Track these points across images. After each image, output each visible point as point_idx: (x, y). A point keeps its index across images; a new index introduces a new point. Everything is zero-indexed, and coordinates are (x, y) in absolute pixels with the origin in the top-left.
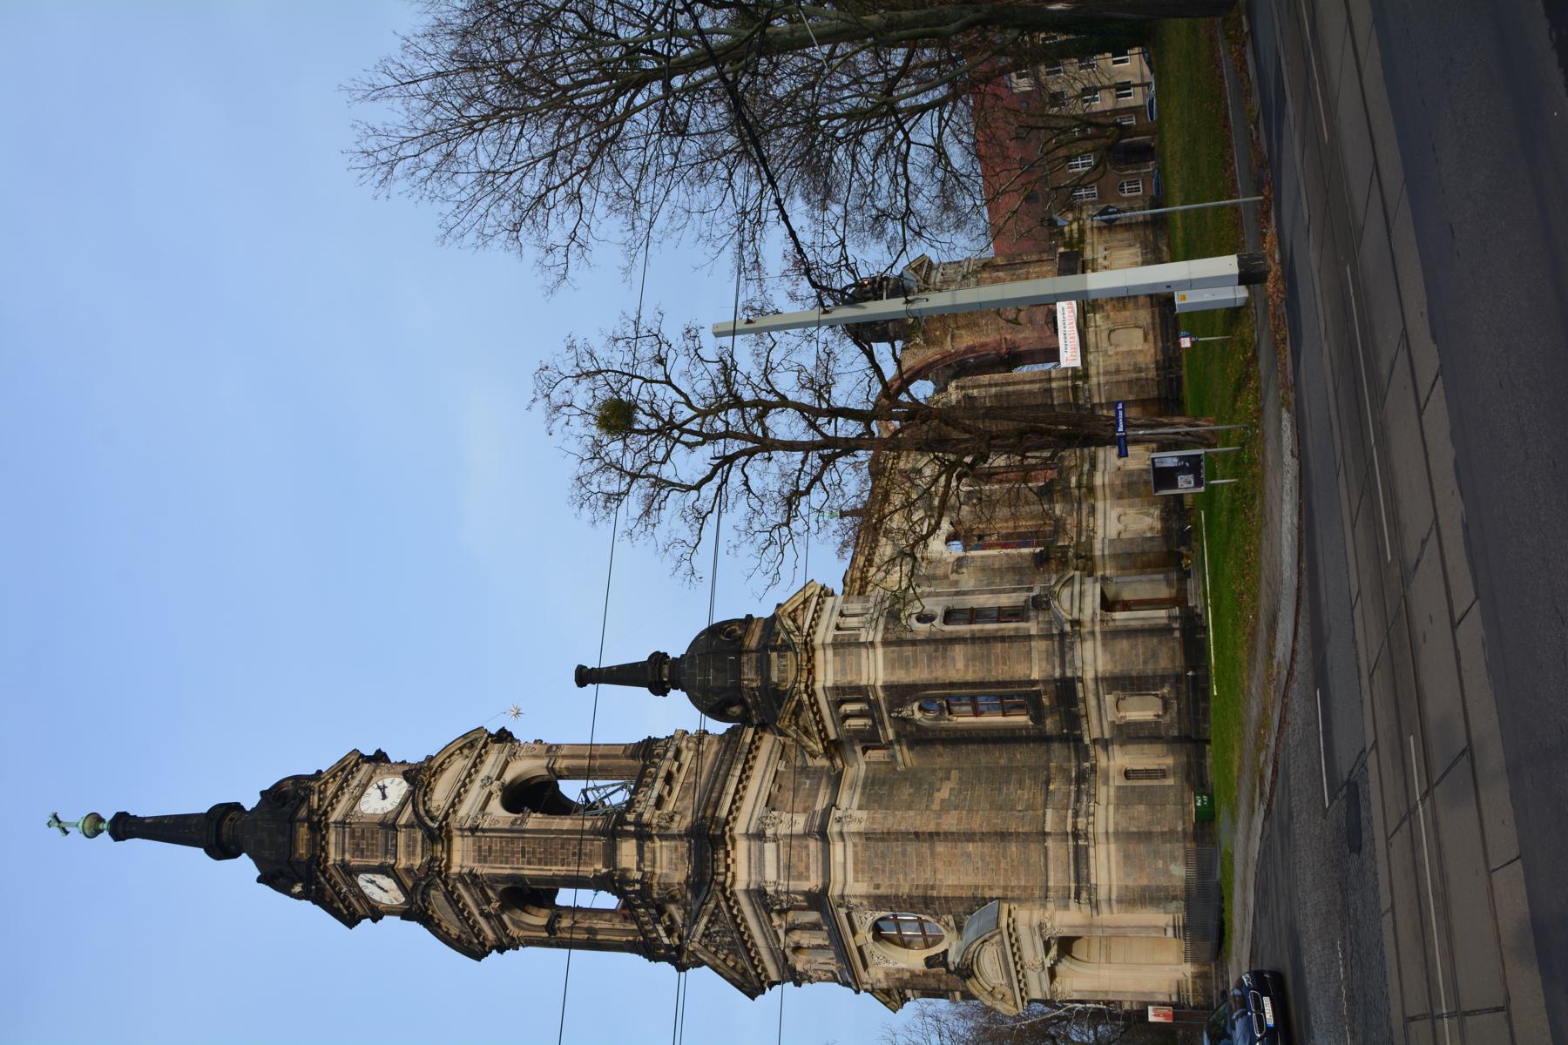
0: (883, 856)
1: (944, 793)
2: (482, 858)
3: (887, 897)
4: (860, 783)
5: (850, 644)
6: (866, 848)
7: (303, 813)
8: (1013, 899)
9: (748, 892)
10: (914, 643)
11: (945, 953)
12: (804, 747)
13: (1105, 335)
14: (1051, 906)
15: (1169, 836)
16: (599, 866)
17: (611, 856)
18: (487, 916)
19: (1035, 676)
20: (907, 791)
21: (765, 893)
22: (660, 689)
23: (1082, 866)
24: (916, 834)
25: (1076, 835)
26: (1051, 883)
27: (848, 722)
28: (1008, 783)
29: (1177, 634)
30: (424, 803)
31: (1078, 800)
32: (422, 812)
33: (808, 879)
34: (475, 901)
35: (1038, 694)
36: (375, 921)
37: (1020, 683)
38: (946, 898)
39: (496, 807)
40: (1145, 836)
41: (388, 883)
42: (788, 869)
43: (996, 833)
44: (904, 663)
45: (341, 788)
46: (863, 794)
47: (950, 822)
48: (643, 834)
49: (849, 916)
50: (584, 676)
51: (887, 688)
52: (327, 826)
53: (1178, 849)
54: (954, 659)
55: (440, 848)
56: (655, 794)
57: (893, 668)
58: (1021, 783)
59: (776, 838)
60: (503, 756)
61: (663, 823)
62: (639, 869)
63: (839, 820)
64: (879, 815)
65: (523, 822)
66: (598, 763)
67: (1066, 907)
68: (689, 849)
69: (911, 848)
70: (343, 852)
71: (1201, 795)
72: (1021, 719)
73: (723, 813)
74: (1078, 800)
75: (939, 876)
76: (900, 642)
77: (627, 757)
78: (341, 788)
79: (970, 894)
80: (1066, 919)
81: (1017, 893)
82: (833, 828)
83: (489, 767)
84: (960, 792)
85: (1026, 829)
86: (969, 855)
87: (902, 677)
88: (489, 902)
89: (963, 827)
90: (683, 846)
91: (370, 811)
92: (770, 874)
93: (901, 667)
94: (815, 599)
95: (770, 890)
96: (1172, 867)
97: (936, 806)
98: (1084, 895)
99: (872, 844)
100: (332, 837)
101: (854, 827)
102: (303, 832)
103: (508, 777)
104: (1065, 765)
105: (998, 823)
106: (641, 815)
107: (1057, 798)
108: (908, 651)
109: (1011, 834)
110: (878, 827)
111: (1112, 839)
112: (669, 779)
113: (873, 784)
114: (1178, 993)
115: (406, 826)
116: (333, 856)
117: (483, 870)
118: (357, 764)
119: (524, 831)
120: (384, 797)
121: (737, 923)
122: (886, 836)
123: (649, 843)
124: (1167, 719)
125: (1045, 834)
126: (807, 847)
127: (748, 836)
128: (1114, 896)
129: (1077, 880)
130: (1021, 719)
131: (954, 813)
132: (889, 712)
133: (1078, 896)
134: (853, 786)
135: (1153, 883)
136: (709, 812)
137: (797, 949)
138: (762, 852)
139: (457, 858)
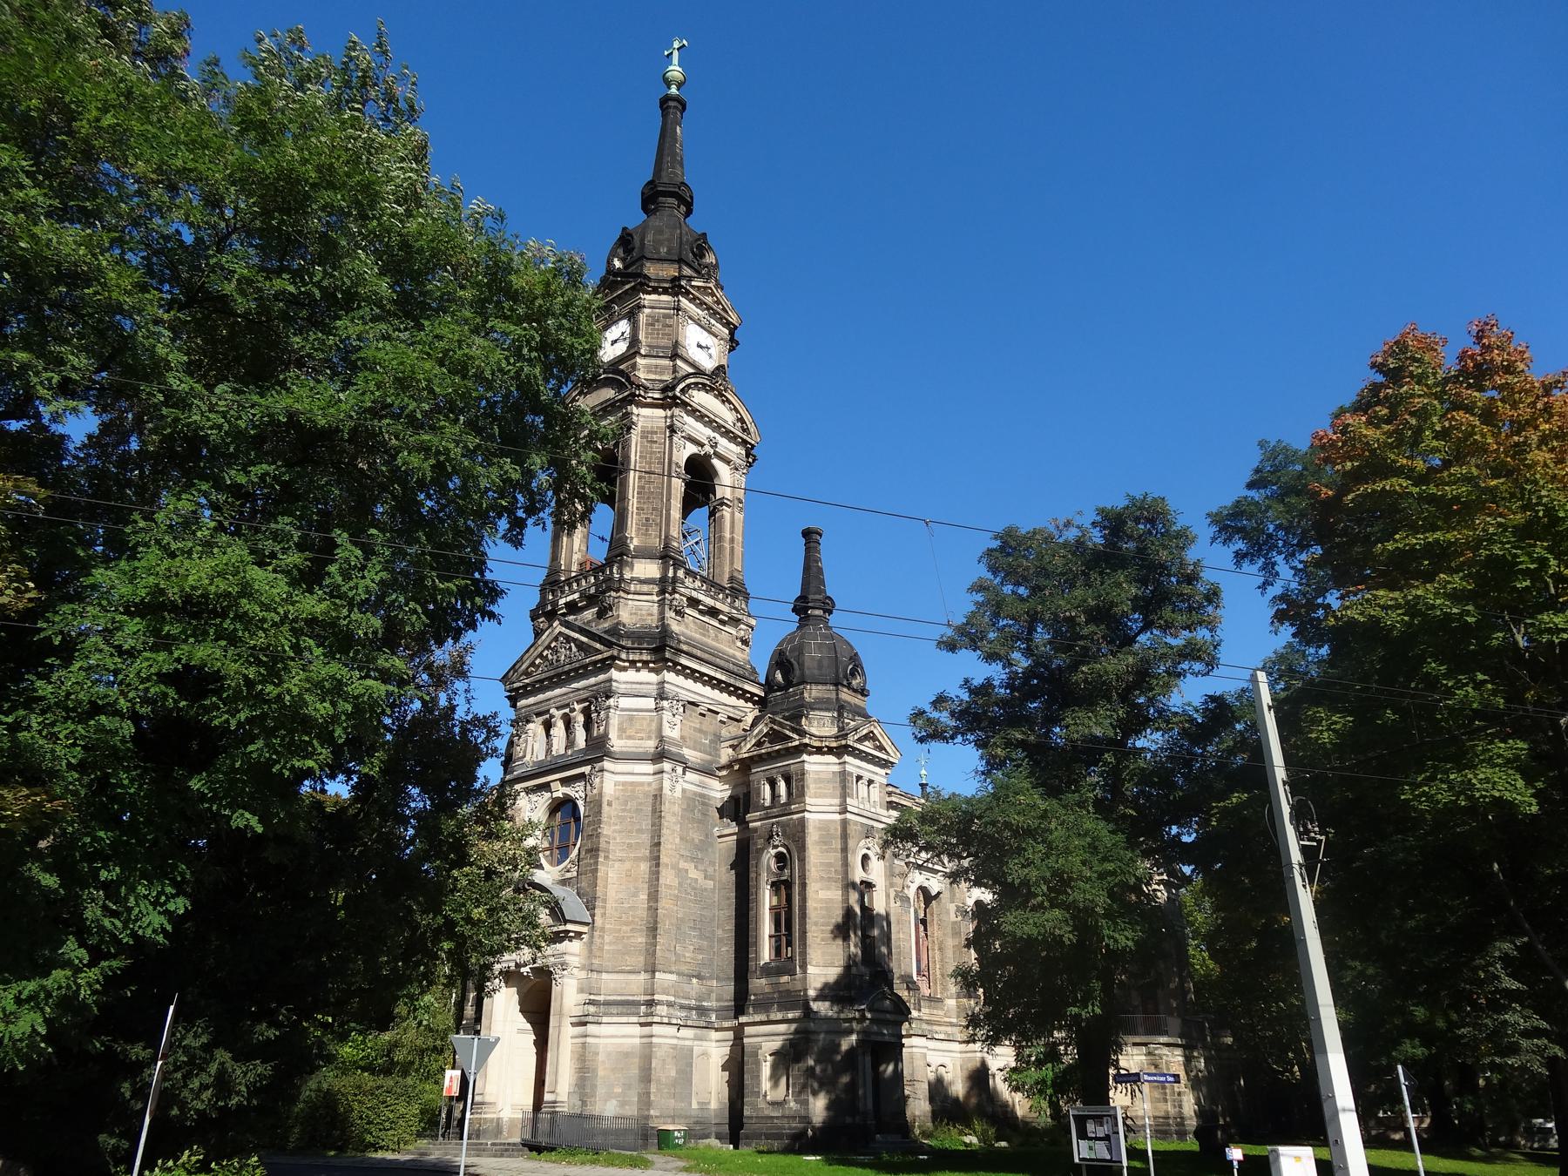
1: (694, 874)
2: (645, 434)
4: (705, 791)
5: (844, 788)
6: (646, 794)
7: (687, 271)
8: (592, 937)
9: (610, 680)
10: (845, 850)
11: (541, 867)
14: (583, 974)
15: (645, 1100)
16: (636, 542)
19: (810, 969)
20: (697, 836)
21: (608, 697)
24: (659, 844)
26: (604, 976)
27: (767, 787)
28: (701, 937)
29: (849, 1120)
30: (696, 384)
31: (682, 1007)
32: (688, 381)
33: (620, 737)
35: (792, 973)
37: (804, 954)
38: (596, 870)
39: (691, 449)
40: (646, 1076)
41: (622, 348)
42: (631, 716)
43: (656, 922)
44: (824, 841)
45: (709, 308)
47: (668, 877)
48: (665, 586)
49: (582, 776)
51: (802, 821)
52: (676, 294)
53: (632, 1110)
56: (701, 597)
57: (820, 829)
58: (699, 950)
60: (734, 458)
62: (632, 579)
64: (676, 808)
66: (727, 545)
67: (581, 991)
69: (645, 838)
72: (766, 954)
74: (682, 1007)
75: (617, 864)
76: (845, 836)
77: (731, 572)
78: (709, 308)
79: (599, 894)
80: (568, 996)
81: (597, 940)
82: (667, 766)
83: (725, 445)
85: (659, 953)
86: (635, 895)
87: (812, 837)
89: (662, 889)
93: (821, 836)
95: (611, 702)
96: (614, 1102)
97: (682, 865)
98: (592, 1009)
99: (650, 800)
100: (665, 298)
101: (667, 784)
102: (671, 271)
103: (716, 462)
104: (714, 996)
107: (686, 987)
108: (837, 844)
109: (655, 937)
110: (666, 807)
112: (713, 612)
113: (704, 804)
116: (648, 299)
117: (635, 437)
119: (670, 476)
120: (699, 346)
121: (582, 672)
122: (657, 814)
123: (656, 589)
124: (762, 1105)
125: (653, 972)
126: (649, 738)
128: (589, 1040)
129: (607, 1003)
130: (766, 954)
131: (676, 883)
133: (591, 1003)
135: (599, 1082)
136: (685, 648)
137: (548, 726)
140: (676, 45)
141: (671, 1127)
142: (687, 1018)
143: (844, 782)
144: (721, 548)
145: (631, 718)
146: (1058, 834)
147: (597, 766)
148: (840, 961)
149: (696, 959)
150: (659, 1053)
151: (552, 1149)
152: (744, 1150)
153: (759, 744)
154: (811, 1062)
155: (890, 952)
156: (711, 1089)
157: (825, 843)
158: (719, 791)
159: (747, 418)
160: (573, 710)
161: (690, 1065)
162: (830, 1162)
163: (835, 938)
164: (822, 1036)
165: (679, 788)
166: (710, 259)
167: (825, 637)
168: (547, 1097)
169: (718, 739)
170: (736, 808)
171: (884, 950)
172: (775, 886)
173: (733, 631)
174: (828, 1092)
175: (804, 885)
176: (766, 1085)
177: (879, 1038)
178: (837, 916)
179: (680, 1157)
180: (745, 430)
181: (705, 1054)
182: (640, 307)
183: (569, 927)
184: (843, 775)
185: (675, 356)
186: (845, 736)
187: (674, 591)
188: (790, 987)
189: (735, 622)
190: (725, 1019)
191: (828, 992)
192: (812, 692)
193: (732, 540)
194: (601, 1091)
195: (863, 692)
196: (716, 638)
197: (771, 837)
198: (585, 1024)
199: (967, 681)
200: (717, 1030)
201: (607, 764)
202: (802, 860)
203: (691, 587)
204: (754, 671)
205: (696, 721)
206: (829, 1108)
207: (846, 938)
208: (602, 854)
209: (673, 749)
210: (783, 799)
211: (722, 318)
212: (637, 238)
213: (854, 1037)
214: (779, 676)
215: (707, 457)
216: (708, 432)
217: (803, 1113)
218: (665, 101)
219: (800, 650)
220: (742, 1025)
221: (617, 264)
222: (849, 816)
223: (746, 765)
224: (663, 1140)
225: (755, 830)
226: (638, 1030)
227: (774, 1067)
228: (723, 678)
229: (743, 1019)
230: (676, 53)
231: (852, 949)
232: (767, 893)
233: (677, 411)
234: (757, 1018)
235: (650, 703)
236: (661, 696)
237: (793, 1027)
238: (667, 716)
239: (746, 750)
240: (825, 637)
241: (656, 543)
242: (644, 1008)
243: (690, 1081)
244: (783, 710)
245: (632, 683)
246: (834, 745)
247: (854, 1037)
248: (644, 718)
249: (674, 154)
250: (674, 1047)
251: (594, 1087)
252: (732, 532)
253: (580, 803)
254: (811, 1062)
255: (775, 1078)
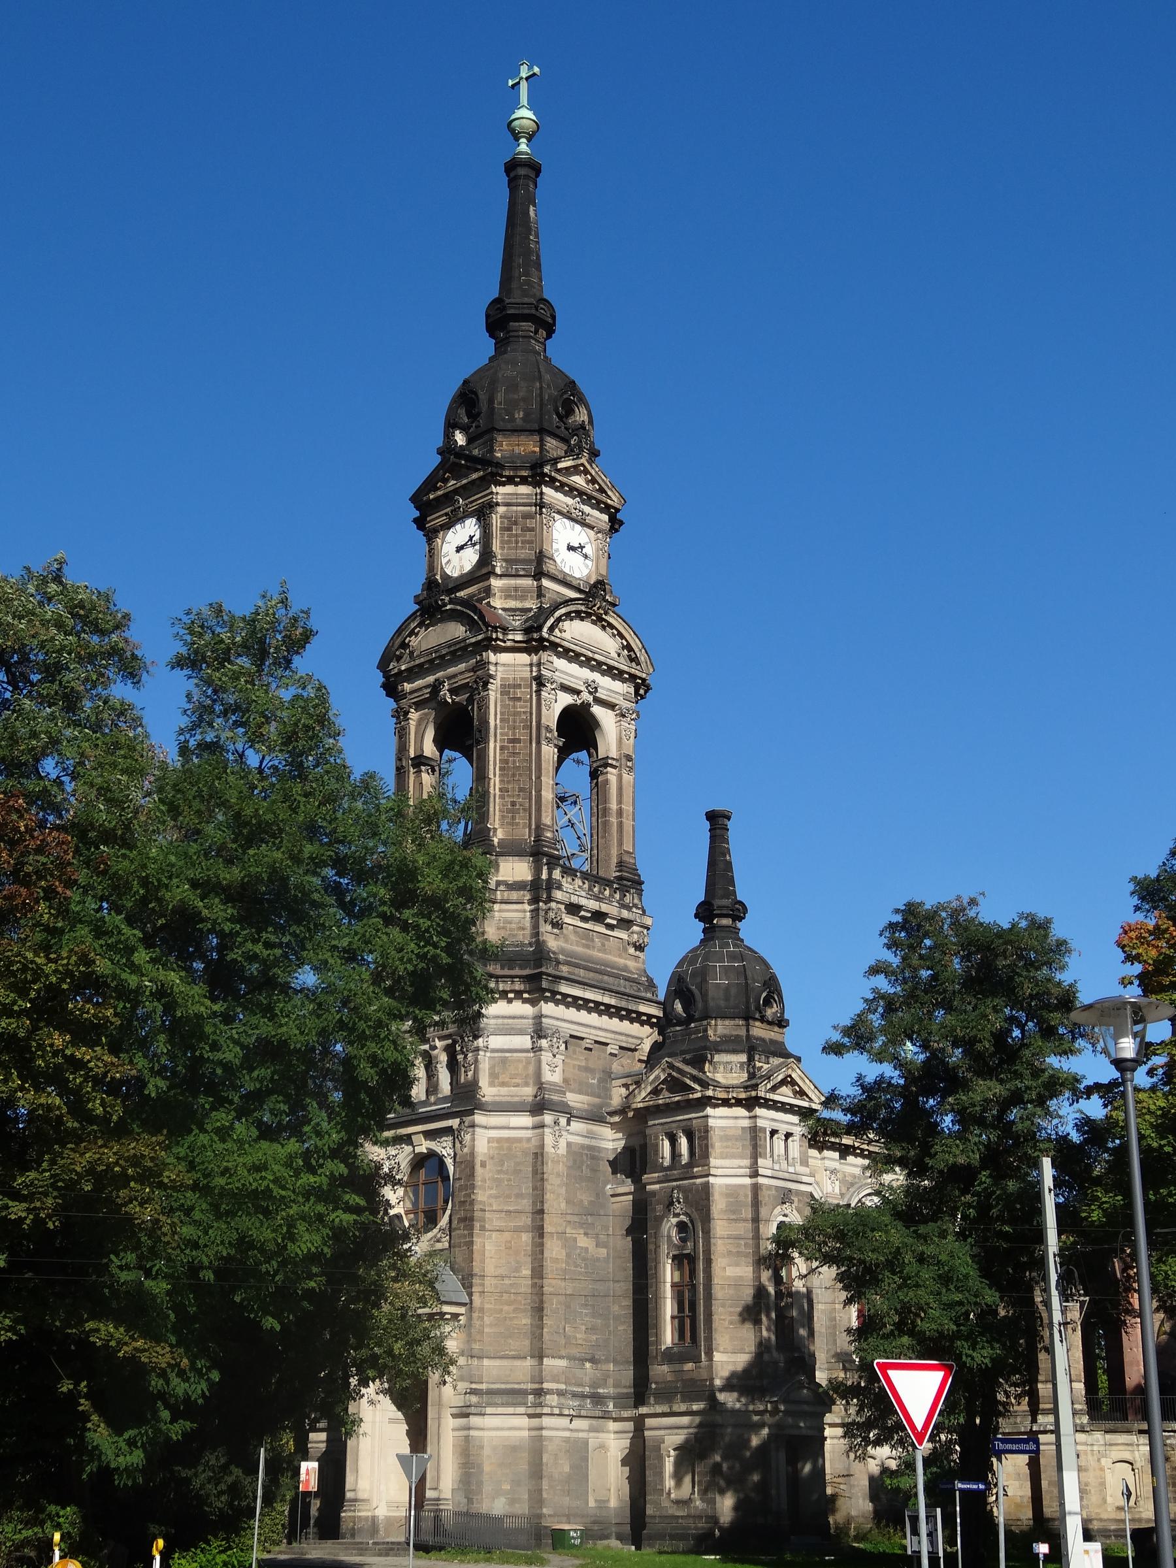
0: (517, 1172)
1: (583, 1242)
3: (472, 1175)
4: (594, 1143)
5: (755, 1147)
7: (551, 443)
8: (470, 1319)
10: (756, 1220)
12: (638, 1083)
13: (1127, 1456)
15: (537, 1498)
17: (512, 849)
18: (436, 687)
19: (717, 1357)
20: (585, 1198)
21: (476, 1037)
22: (705, 912)
23: (505, 1398)
25: (539, 1393)
26: (486, 1362)
27: (667, 1143)
28: (594, 1315)
30: (568, 614)
31: (575, 1395)
32: (557, 614)
33: (492, 1084)
34: (454, 676)
35: (697, 1360)
36: (415, 521)
37: (709, 1339)
39: (565, 699)
40: (537, 1471)
41: (470, 558)
42: (503, 1059)
43: (542, 1302)
44: (733, 1208)
46: (583, 1146)
47: (554, 1250)
48: (539, 891)
49: (449, 1131)
50: (717, 820)
51: (706, 1188)
52: (537, 484)
53: (522, 1508)
54: (737, 1265)
55: (519, 638)
56: (583, 902)
57: (727, 1195)
58: (592, 1329)
59: (536, 1049)
61: (551, 915)
62: (498, 883)
63: (556, 1123)
64: (561, 1168)
65: (549, 740)
66: (613, 820)
68: (522, 945)
69: (526, 1204)
70: (508, 505)
71: (581, 1537)
72: (668, 1337)
73: (565, 988)
74: (575, 1395)
75: (494, 1234)
76: (756, 1204)
77: (620, 855)
78: (581, 493)
79: (476, 1270)
81: (476, 1323)
82: (548, 1118)
84: (584, 1259)
85: (546, 1337)
87: (718, 1205)
88: (452, 691)
89: (548, 1264)
90: (524, 936)
91: (555, 535)
92: (496, 1042)
94: (805, 1104)
95: (480, 1042)
96: (503, 1500)
98: (474, 1399)
99: (530, 1159)
100: (524, 489)
101: (549, 1140)
103: (597, 710)
104: (611, 1381)
105: (552, 1305)
106: (560, 888)
107: (579, 1373)
108: (747, 1213)
110: (549, 1167)
111: (534, 1433)
112: (598, 916)
113: (593, 1158)
114: (355, 1500)
115: (540, 587)
116: (502, 492)
117: (493, 693)
118: (608, 507)
119: (539, 743)
120: (570, 548)
122: (539, 1177)
123: (528, 897)
124: (665, 1503)
125: (540, 1356)
126: (526, 1084)
127: (539, 1017)
128: (472, 1433)
129: (490, 1392)
130: (668, 1337)
132: (678, 1187)
133: (473, 1392)
134: (590, 1135)
135: (485, 1478)
138: (521, 1032)
139: (504, 658)
140: (524, 73)
141: (566, 1527)
142: (581, 1407)
143: (755, 1140)
144: (606, 823)
145: (504, 1061)
146: (911, 1268)
147: (467, 1120)
148: (751, 1347)
149: (587, 1338)
150: (550, 1447)
151: (441, 1549)
152: (646, 1550)
153: (656, 1092)
154: (718, 1458)
155: (811, 1333)
156: (610, 1483)
157: (734, 1212)
158: (611, 1141)
159: (635, 644)
160: (434, 1048)
161: (586, 1459)
162: (724, 1560)
163: (743, 1321)
164: (729, 1430)
165: (563, 1144)
166: (581, 416)
167: (733, 957)
168: (429, 1494)
169: (608, 1076)
170: (633, 1162)
171: (803, 1332)
172: (678, 1260)
173: (623, 935)
174: (736, 1491)
175: (708, 1262)
176: (669, 1483)
177: (795, 1432)
178: (748, 1294)
179: (576, 1557)
180: (633, 659)
181: (602, 1447)
182: (492, 506)
183: (446, 1309)
184: (754, 1131)
185: (539, 575)
186: (755, 1087)
187: (550, 899)
188: (695, 1375)
189: (625, 924)
190: (625, 1407)
191: (736, 1382)
192: (718, 1029)
193: (620, 813)
194: (487, 1488)
195: (781, 1023)
196: (603, 949)
197: (671, 1203)
198: (467, 1415)
199: (860, 1078)
200: (615, 1420)
201: (479, 1118)
202: (707, 1232)
203: (571, 890)
204: (651, 985)
205: (581, 1059)
206: (736, 1508)
207: (757, 1322)
208: (477, 1225)
209: (555, 1097)
210: (685, 1159)
211: (599, 502)
212: (483, 396)
213: (766, 1431)
214: (678, 1006)
215: (586, 706)
216: (586, 674)
217: (710, 1512)
218: (512, 166)
219: (703, 974)
220: (643, 1417)
221: (460, 439)
222: (761, 1180)
223: (644, 1114)
224: (559, 1540)
225: (653, 1193)
226: (525, 1421)
227: (678, 1464)
228: (613, 1002)
229: (643, 1410)
230: (524, 86)
231: (765, 1333)
232: (668, 1267)
233: (545, 656)
234: (659, 1409)
235: (525, 1041)
236: (539, 1032)
237: (697, 1419)
238: (546, 1057)
239: (641, 1099)
240: (733, 957)
241: (525, 835)
242: (531, 1397)
243: (586, 1477)
244: (683, 1052)
245: (503, 1013)
246: (743, 1096)
247: (766, 1431)
248: (519, 1061)
249: (528, 252)
250: (567, 1440)
251: (480, 1484)
252: (620, 802)
253: (449, 1162)
254: (718, 1458)
255: (678, 1477)
